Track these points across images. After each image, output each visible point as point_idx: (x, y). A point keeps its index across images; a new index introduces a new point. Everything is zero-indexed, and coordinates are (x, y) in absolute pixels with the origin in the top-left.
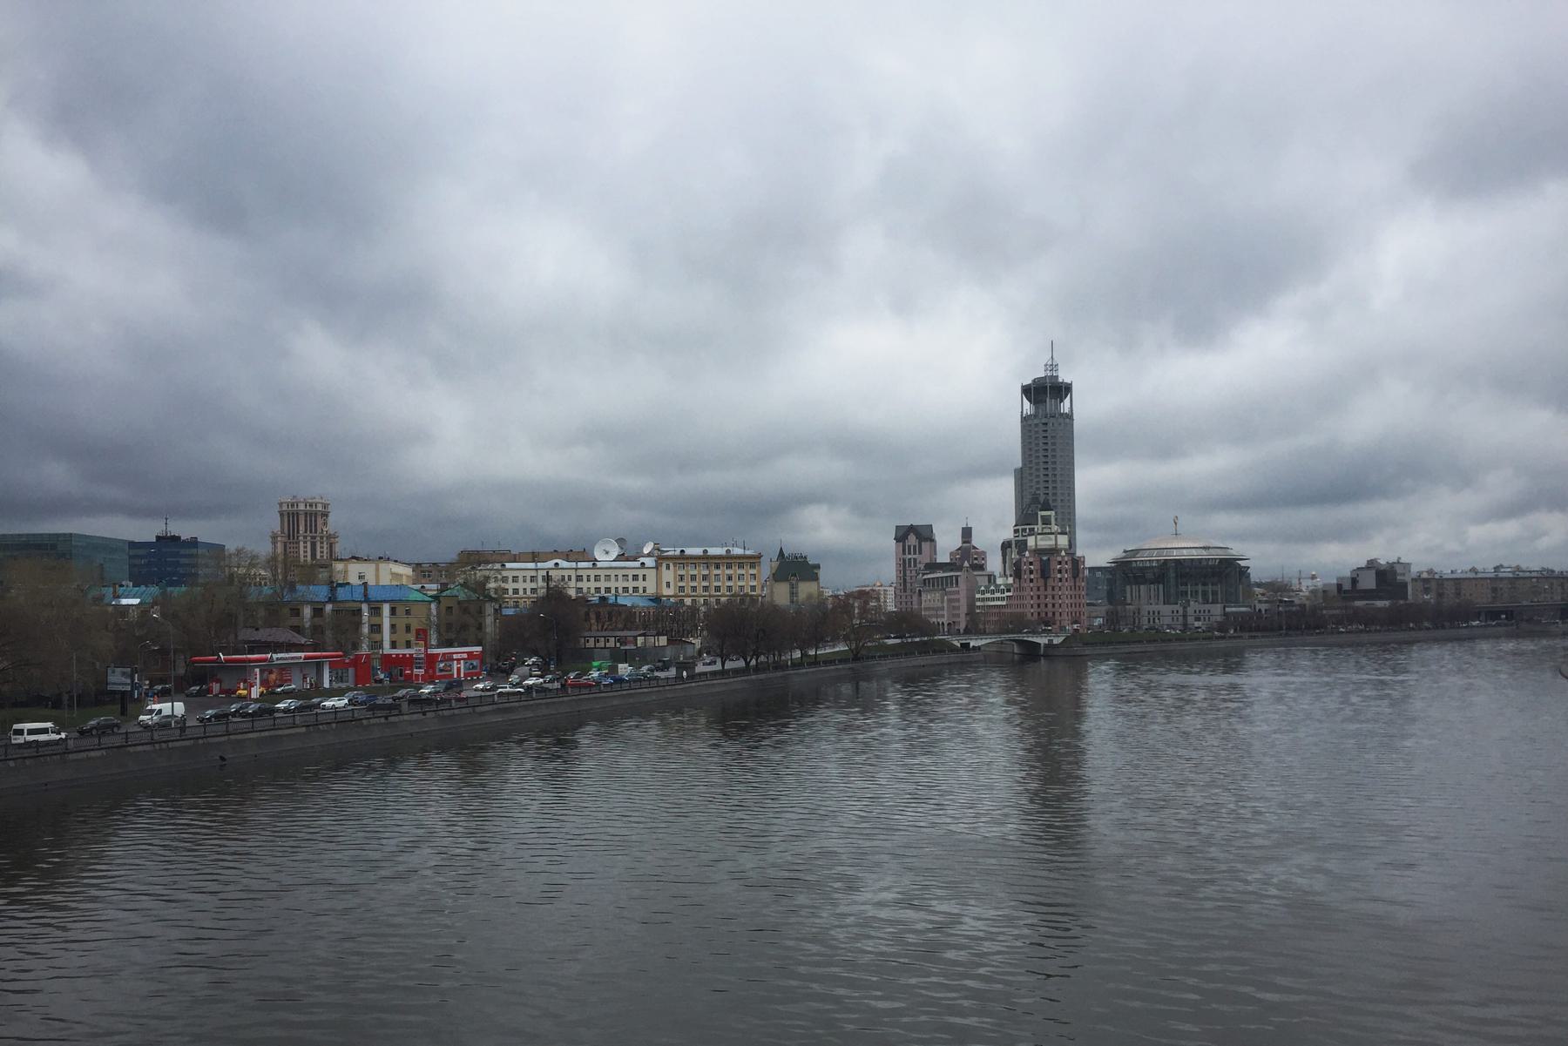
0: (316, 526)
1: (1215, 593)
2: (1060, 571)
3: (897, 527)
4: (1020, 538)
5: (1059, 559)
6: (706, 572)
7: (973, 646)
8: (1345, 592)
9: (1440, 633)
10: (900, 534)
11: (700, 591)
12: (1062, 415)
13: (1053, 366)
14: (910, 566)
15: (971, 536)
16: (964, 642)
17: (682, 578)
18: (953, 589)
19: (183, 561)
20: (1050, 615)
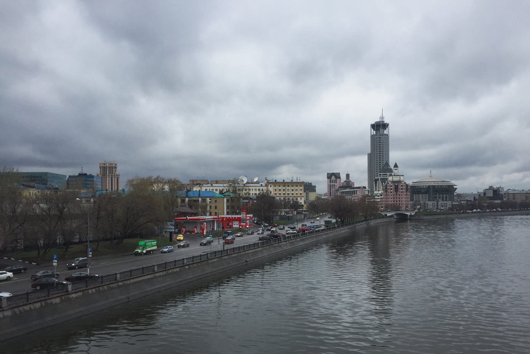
0: (112, 171)
1: (446, 197)
2: (402, 189)
3: (340, 173)
4: (382, 177)
5: (402, 185)
6: (284, 188)
7: (389, 216)
8: (481, 197)
9: (520, 212)
10: (329, 175)
11: (282, 195)
12: (385, 134)
13: (382, 118)
14: (332, 187)
15: (349, 177)
16: (385, 214)
17: (276, 190)
18: (355, 195)
19: (88, 182)
20: (398, 204)
